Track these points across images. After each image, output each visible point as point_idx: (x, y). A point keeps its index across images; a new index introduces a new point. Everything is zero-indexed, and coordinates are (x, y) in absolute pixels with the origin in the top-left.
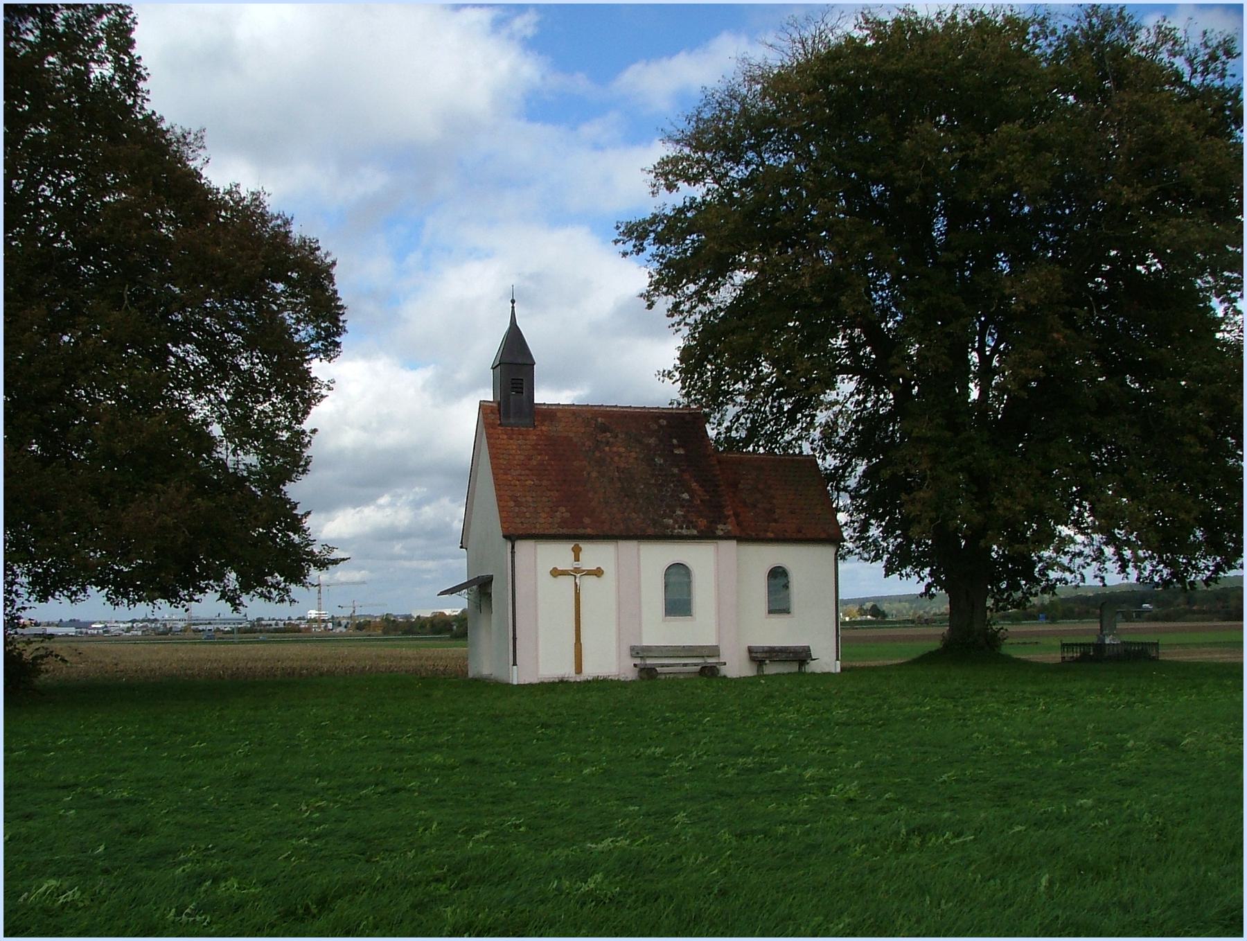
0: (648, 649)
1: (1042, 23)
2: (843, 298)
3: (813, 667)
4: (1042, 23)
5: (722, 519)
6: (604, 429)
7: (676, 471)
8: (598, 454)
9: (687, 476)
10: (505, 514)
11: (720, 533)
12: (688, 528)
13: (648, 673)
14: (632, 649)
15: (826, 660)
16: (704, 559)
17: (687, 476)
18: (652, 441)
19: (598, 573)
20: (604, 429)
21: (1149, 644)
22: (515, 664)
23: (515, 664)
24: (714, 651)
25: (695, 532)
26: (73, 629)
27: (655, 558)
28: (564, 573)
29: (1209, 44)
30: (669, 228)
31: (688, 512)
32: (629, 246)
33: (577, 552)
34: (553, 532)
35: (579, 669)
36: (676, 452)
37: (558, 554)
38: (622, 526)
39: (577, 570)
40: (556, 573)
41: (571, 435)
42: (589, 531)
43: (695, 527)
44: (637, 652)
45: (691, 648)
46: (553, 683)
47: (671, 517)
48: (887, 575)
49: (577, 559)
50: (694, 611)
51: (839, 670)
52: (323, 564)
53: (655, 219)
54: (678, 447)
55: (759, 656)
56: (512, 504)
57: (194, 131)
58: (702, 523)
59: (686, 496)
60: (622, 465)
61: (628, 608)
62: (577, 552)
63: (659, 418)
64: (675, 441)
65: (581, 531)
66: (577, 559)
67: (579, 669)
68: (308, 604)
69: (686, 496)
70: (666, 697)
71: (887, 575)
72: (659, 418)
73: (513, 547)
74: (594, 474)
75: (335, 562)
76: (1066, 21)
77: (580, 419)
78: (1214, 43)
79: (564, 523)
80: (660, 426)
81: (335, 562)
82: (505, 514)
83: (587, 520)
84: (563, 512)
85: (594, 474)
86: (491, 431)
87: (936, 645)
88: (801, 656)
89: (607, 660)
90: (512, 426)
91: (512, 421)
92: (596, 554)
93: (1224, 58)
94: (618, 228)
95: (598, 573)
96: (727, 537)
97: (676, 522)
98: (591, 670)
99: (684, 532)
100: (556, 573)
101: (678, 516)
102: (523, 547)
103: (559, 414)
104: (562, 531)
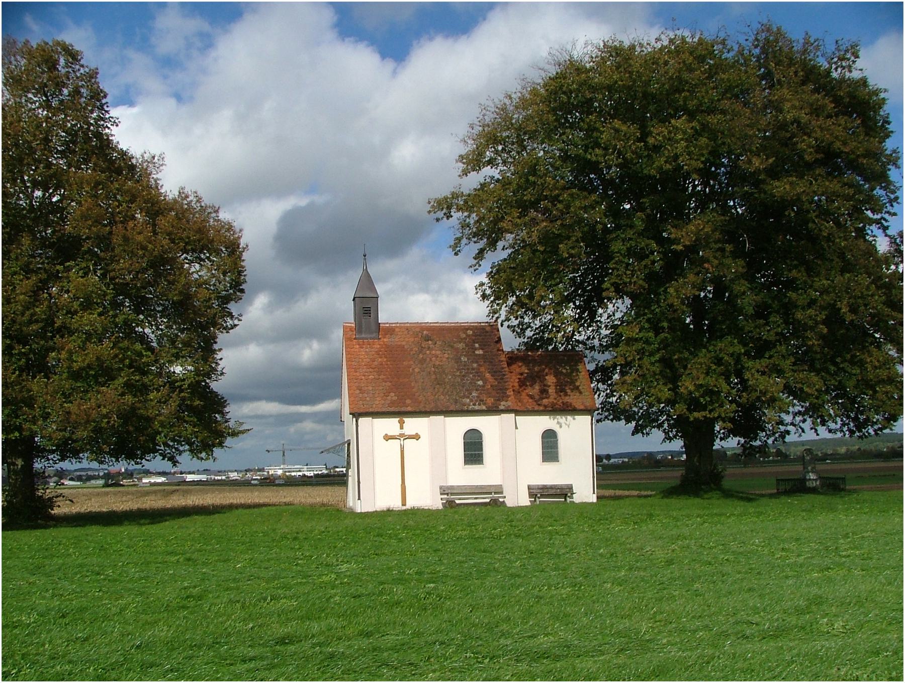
0: (452, 487)
1: (723, 42)
2: (561, 246)
3: (577, 499)
4: (723, 42)
5: (505, 397)
6: (427, 339)
7: (475, 365)
8: (421, 356)
9: (482, 369)
10: (352, 399)
11: (502, 407)
12: (479, 405)
13: (450, 504)
14: (441, 488)
15: (585, 491)
16: (491, 427)
17: (482, 369)
18: (461, 346)
19: (417, 437)
20: (427, 339)
21: (837, 479)
22: (359, 499)
23: (359, 499)
24: (499, 490)
25: (484, 408)
26: (205, 476)
27: (456, 427)
28: (393, 438)
29: (841, 48)
30: (470, 203)
31: (481, 393)
32: (440, 214)
33: (402, 423)
34: (384, 410)
35: (404, 504)
36: (477, 352)
37: (390, 425)
38: (433, 405)
39: (402, 435)
40: (387, 438)
41: (404, 343)
42: (409, 409)
43: (484, 404)
44: (444, 491)
45: (481, 487)
46: (383, 511)
47: (468, 397)
48: (633, 434)
49: (402, 428)
50: (560, 459)
51: (595, 500)
52: (234, 434)
53: (455, 196)
54: (479, 349)
55: (536, 492)
56: (358, 392)
57: (158, 154)
58: (490, 401)
59: (480, 383)
60: (437, 363)
61: (439, 460)
62: (402, 423)
63: (467, 329)
64: (477, 345)
65: (403, 409)
66: (402, 428)
67: (404, 504)
68: (229, 459)
69: (480, 383)
70: (471, 519)
71: (633, 434)
72: (467, 329)
73: (357, 421)
74: (417, 370)
75: (243, 432)
76: (742, 40)
77: (411, 333)
78: (844, 47)
79: (392, 403)
80: (468, 336)
81: (243, 432)
82: (352, 399)
83: (408, 401)
84: (393, 396)
85: (417, 370)
86: (348, 343)
87: (676, 482)
88: (565, 492)
89: (424, 496)
90: (363, 339)
91: (363, 336)
92: (413, 424)
93: (853, 58)
94: (429, 203)
95: (417, 437)
96: (507, 411)
97: (472, 400)
98: (410, 504)
99: (477, 408)
100: (387, 438)
101: (473, 397)
102: (362, 420)
103: (397, 330)
104: (392, 409)
